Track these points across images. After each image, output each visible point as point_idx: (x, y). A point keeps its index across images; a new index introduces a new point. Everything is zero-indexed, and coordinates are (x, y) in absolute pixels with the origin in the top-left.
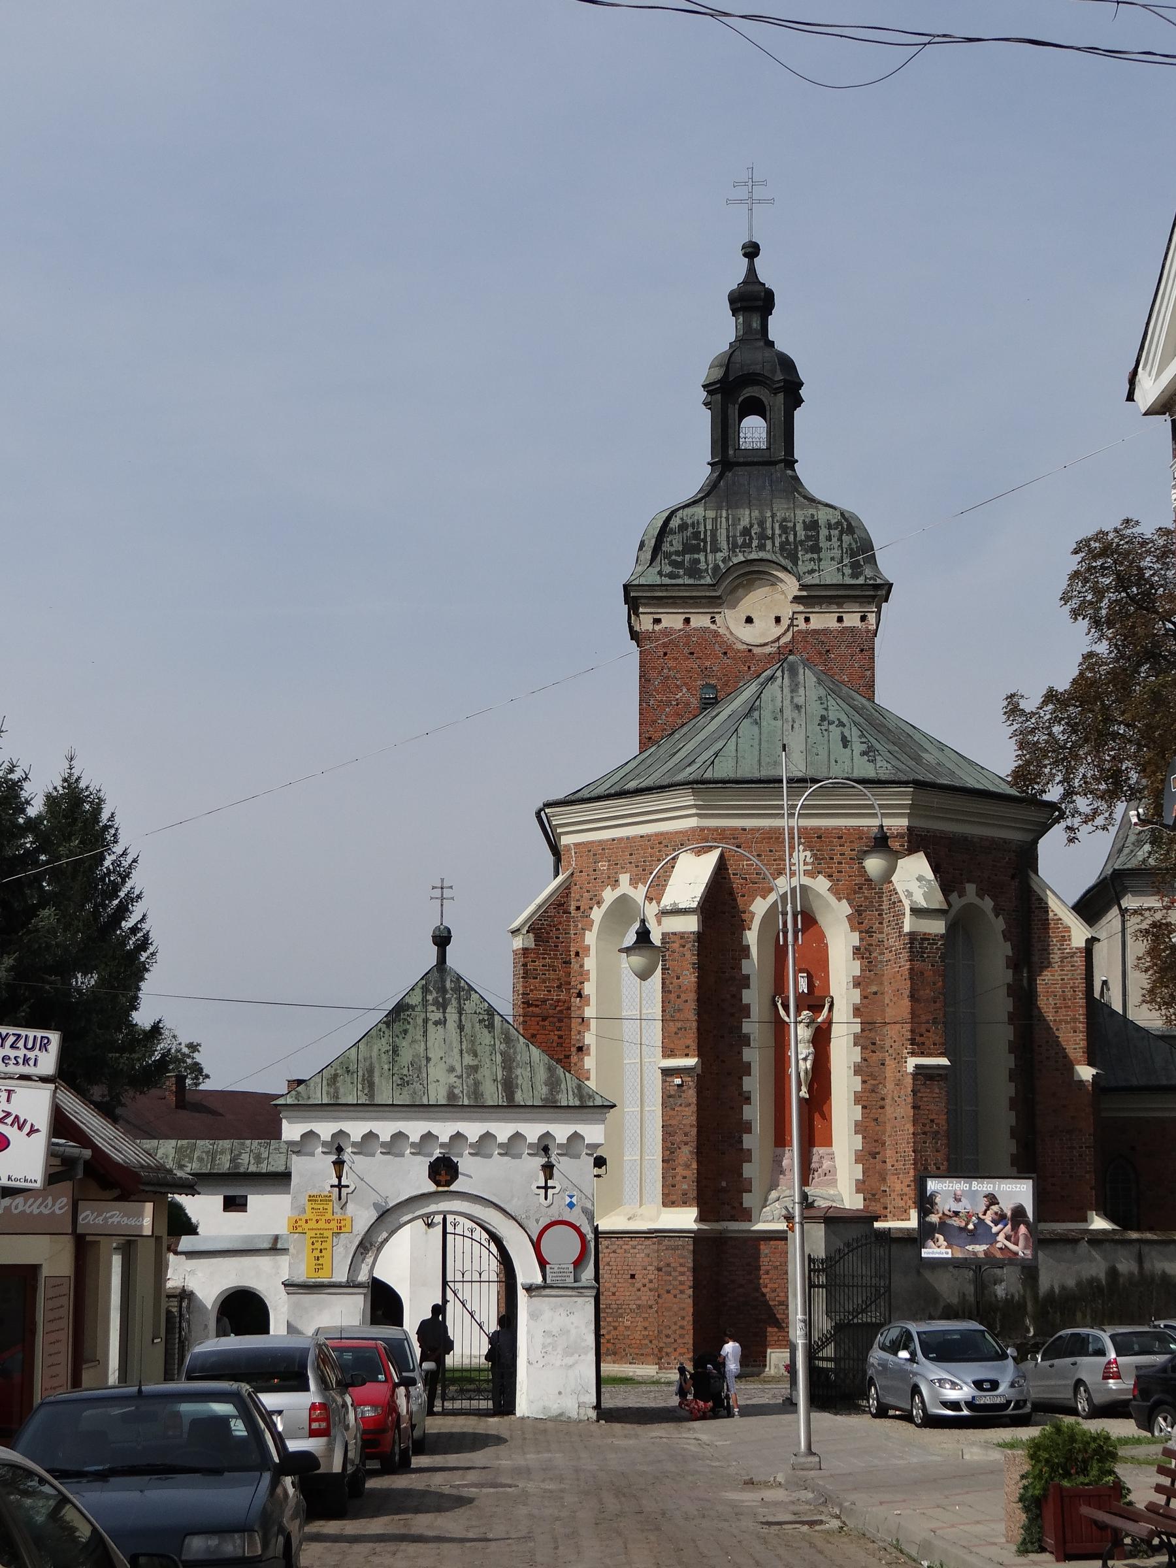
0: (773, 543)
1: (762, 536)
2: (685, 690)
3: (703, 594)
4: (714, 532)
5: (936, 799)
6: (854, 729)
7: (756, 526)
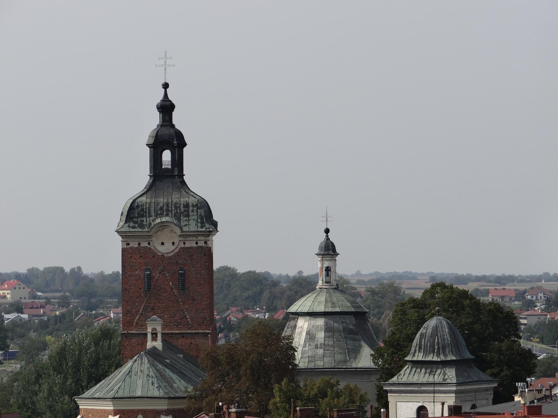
1: (168, 210)
4: (149, 208)
5: (172, 401)
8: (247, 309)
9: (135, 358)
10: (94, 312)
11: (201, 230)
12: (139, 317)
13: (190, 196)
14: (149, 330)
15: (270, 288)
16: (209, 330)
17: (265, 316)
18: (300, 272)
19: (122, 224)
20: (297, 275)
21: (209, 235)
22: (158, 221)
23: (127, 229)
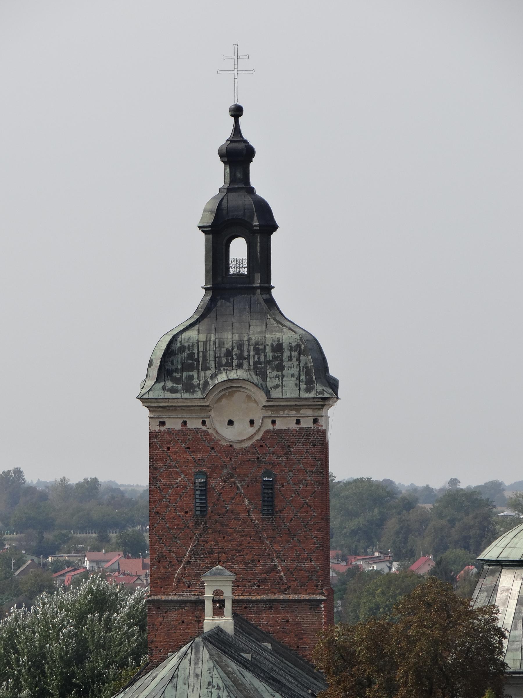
0: (249, 364)
1: (241, 357)
2: (183, 476)
3: (196, 404)
4: (205, 352)
6: (225, 691)
7: (236, 349)
8: (356, 553)
9: (184, 649)
10: (50, 559)
11: (307, 396)
12: (184, 568)
13: (285, 330)
14: (209, 594)
15: (399, 513)
16: (321, 594)
17: (390, 568)
18: (454, 482)
19: (150, 383)
20: (447, 487)
21: (323, 406)
22: (222, 377)
23: (161, 394)
